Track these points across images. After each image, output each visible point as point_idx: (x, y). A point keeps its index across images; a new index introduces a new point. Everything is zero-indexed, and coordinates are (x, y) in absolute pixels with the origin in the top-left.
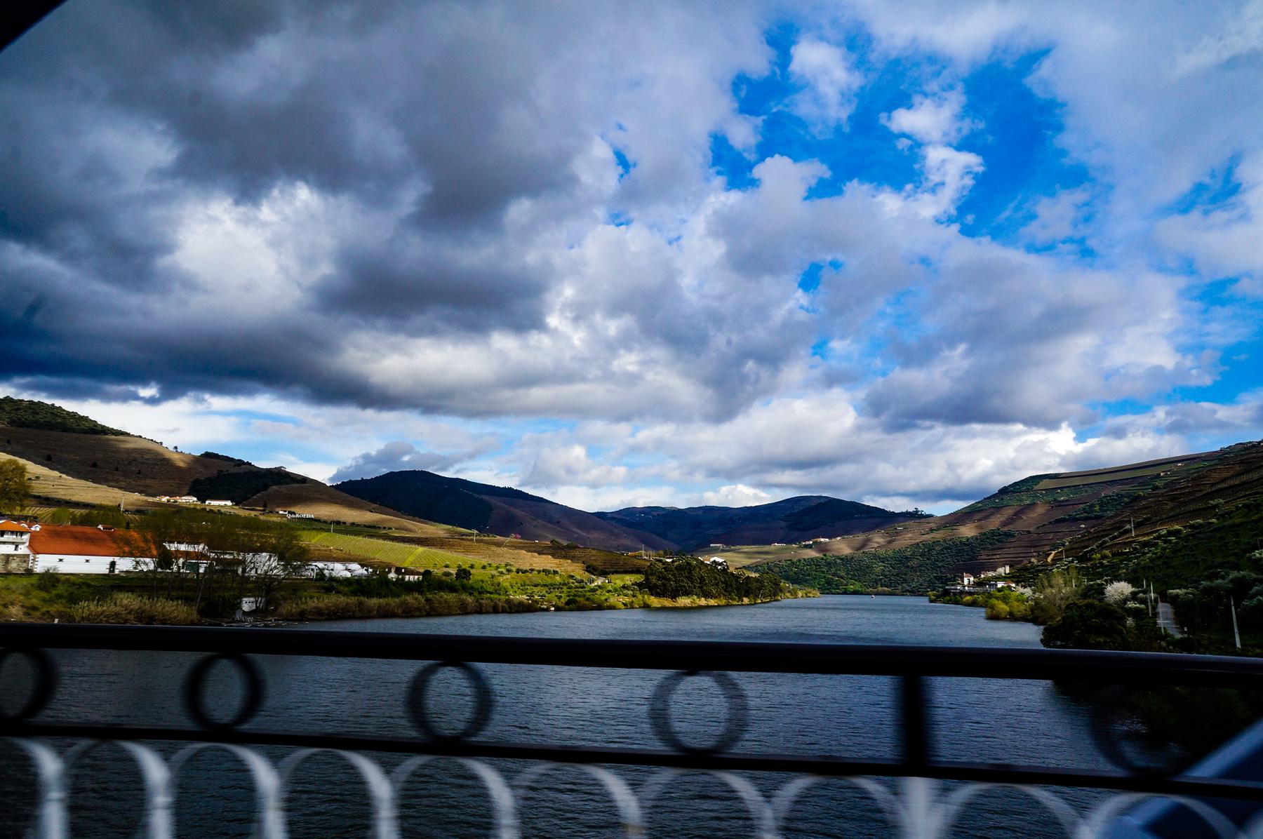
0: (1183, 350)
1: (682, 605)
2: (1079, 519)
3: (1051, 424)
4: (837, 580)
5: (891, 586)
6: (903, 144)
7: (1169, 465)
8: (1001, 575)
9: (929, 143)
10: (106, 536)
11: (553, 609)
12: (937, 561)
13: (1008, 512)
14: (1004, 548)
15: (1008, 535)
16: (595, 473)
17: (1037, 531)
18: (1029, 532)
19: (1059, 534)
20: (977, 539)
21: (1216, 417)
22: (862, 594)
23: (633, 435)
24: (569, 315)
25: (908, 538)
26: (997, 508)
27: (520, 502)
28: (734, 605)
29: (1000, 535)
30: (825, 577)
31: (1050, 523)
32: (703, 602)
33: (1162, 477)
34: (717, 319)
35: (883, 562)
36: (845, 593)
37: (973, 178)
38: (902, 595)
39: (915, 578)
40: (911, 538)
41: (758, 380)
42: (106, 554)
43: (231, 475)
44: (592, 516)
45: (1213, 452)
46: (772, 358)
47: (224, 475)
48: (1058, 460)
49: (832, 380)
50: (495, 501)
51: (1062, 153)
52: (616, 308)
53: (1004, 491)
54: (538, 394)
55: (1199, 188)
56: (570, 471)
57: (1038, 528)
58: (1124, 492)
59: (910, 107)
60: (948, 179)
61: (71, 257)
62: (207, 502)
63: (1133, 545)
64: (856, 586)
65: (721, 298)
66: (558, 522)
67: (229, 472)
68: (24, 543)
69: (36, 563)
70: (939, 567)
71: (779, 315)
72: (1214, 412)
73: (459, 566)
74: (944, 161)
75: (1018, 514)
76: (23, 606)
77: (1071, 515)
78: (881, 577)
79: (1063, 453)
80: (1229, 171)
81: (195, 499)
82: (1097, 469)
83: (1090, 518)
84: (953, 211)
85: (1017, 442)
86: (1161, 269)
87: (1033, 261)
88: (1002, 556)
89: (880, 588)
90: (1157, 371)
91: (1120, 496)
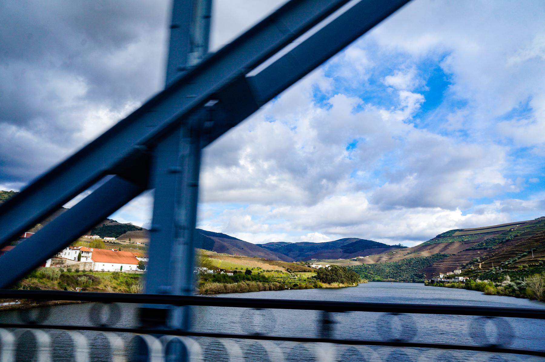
0: (506, 177)
1: (334, 287)
2: (477, 249)
3: (452, 208)
4: (370, 275)
5: (394, 278)
6: (390, 90)
7: (513, 226)
8: (458, 274)
9: (401, 90)
10: (116, 254)
11: (289, 289)
12: (414, 267)
13: (443, 246)
14: (444, 262)
15: (444, 256)
16: (255, 227)
17: (458, 254)
18: (454, 255)
19: (468, 256)
20: (430, 257)
21: (522, 205)
22: (381, 281)
23: (271, 211)
24: (249, 159)
25: (399, 257)
26: (437, 244)
27: (226, 239)
28: (350, 287)
29: (441, 256)
30: (364, 274)
31: (464, 251)
32: (341, 285)
33: (512, 231)
34: (311, 162)
35: (389, 267)
36: (374, 281)
37: (420, 105)
38: (399, 282)
39: (405, 274)
40: (400, 257)
41: (327, 188)
42: (118, 262)
43: (108, 226)
44: (257, 246)
45: (532, 220)
46: (334, 178)
47: (106, 226)
48: (454, 223)
49: (359, 188)
50: (215, 239)
51: (454, 93)
52: (268, 157)
53: (439, 237)
54: (233, 193)
55: (514, 110)
56: (244, 226)
57: (458, 253)
58: (496, 238)
59: (393, 75)
60: (409, 105)
61: (37, 133)
62: (105, 238)
63: (540, 262)
64: (378, 278)
65: (312, 153)
66: (243, 249)
67: (108, 225)
68: (89, 257)
69: (95, 266)
70: (415, 270)
71: (338, 160)
72: (521, 203)
73: (247, 269)
74: (407, 97)
75: (446, 248)
76: (111, 287)
77: (473, 247)
78: (389, 274)
79: (457, 220)
80: (527, 104)
81: (99, 237)
82: (480, 227)
83: (482, 249)
84: (411, 118)
85: (437, 215)
86: (499, 143)
87: (445, 139)
88: (443, 265)
89: (389, 279)
90: (497, 186)
91: (494, 239)
